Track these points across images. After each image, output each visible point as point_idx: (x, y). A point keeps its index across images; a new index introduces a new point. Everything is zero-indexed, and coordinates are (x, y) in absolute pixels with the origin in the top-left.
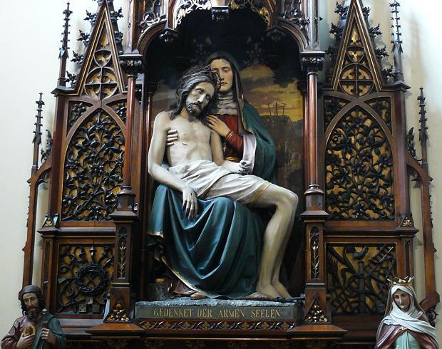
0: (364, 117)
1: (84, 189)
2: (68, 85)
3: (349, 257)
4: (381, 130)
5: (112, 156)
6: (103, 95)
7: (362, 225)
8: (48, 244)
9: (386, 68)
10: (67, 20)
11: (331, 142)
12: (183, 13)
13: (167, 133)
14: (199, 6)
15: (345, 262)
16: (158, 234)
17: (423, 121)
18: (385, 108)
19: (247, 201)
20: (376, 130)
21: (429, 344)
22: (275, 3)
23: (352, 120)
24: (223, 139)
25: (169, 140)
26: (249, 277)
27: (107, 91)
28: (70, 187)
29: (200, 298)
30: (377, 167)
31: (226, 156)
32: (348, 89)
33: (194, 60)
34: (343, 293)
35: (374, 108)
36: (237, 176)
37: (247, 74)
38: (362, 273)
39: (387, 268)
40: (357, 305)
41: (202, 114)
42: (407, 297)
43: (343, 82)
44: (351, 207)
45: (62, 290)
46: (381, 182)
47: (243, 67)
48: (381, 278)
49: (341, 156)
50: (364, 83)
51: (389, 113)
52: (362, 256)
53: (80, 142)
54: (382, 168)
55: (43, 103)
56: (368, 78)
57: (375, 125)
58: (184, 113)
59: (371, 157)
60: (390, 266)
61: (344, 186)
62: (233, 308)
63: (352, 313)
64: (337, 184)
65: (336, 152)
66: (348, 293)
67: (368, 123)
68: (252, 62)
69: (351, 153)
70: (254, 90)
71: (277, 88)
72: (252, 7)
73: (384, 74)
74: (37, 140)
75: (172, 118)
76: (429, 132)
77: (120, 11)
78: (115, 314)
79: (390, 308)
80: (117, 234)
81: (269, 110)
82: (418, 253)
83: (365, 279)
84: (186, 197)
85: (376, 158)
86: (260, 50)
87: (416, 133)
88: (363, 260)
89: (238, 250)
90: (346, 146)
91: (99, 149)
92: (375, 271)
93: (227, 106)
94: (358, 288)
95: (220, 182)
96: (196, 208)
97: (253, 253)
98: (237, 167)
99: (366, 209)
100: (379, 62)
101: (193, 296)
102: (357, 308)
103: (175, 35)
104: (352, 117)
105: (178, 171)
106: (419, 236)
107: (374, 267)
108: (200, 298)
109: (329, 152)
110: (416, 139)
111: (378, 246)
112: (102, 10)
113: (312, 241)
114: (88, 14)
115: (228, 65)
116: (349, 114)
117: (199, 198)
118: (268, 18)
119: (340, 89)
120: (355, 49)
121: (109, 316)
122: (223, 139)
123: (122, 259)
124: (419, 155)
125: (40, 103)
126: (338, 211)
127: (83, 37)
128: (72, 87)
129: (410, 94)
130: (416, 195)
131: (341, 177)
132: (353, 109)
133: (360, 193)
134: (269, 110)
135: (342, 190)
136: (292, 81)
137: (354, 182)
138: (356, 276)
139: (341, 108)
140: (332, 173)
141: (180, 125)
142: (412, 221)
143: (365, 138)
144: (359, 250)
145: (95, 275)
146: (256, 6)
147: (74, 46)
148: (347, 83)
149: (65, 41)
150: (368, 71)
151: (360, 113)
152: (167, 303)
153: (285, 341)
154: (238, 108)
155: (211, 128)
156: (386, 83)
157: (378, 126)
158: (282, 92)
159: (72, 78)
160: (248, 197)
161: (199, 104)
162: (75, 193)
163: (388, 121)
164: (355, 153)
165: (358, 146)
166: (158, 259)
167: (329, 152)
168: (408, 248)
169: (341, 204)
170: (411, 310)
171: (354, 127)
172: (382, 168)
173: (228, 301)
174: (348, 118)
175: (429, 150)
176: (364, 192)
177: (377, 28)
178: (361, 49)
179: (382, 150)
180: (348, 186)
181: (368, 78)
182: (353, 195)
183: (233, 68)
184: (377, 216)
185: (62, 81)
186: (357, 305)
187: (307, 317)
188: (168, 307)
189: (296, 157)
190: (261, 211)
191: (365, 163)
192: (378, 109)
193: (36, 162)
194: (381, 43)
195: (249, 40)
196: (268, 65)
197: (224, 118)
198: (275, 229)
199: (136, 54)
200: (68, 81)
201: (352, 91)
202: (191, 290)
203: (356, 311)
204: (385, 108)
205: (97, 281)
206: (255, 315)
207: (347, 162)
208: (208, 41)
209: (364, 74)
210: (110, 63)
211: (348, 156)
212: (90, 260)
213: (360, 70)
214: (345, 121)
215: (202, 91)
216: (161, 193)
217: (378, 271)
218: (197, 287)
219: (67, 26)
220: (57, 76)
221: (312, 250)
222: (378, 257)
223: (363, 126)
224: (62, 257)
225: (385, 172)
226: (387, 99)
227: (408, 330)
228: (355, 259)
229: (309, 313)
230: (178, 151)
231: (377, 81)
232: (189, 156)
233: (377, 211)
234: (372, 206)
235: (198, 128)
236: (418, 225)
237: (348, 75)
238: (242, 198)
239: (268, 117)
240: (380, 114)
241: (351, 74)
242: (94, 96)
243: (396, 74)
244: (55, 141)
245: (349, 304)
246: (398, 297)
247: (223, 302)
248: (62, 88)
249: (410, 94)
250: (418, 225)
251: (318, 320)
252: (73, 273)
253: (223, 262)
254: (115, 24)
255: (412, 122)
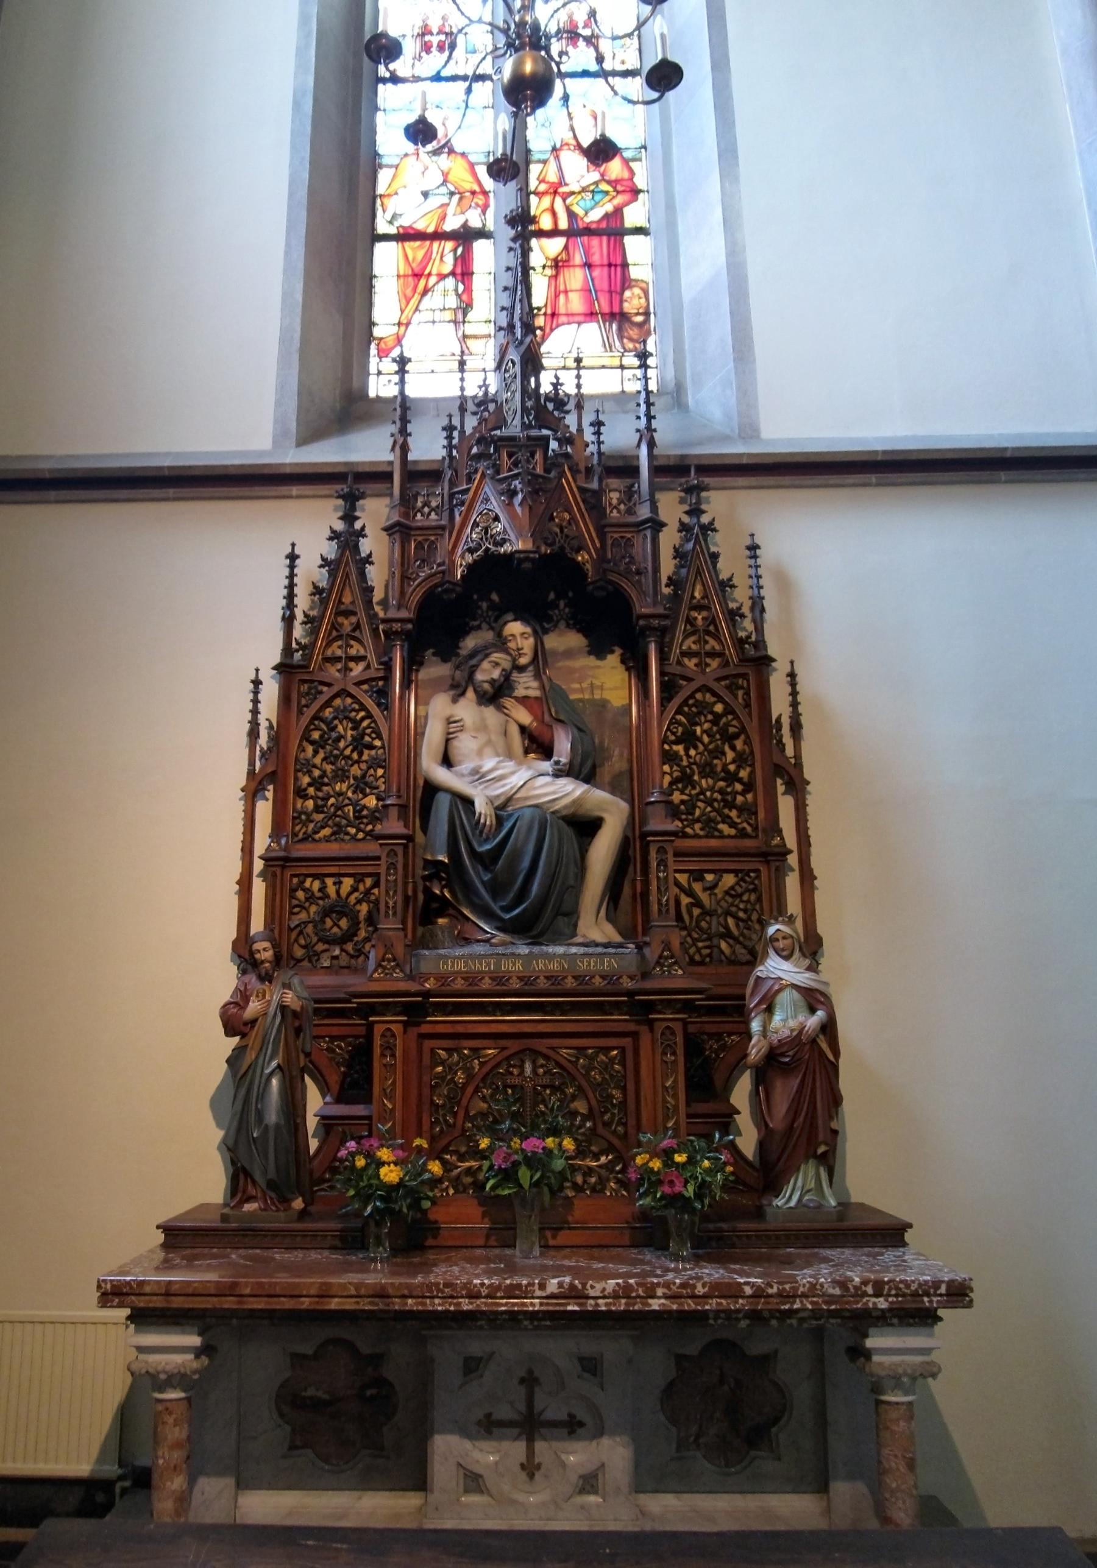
0: (713, 699)
1: (323, 799)
2: (298, 656)
3: (697, 887)
4: (737, 718)
5: (361, 754)
6: (347, 669)
7: (714, 843)
8: (274, 875)
9: (742, 634)
10: (292, 567)
11: (669, 733)
12: (469, 558)
13: (449, 721)
14: (493, 548)
15: (690, 893)
16: (441, 858)
17: (795, 704)
18: (742, 688)
19: (564, 813)
20: (730, 717)
21: (822, 1003)
22: (598, 545)
23: (697, 704)
24: (523, 729)
25: (451, 730)
26: (566, 915)
27: (352, 664)
28: (301, 797)
29: (503, 944)
30: (732, 767)
31: (527, 752)
32: (691, 663)
33: (476, 623)
34: (689, 935)
35: (727, 687)
36: (548, 779)
37: (552, 641)
38: (713, 907)
39: (748, 901)
40: (708, 951)
41: (495, 695)
42: (789, 941)
43: (684, 654)
44: (698, 821)
45: (294, 935)
46: (739, 787)
47: (546, 631)
48: (741, 914)
49: (682, 753)
50: (712, 654)
51: (747, 693)
52: (715, 886)
53: (316, 735)
54: (739, 767)
55: (261, 683)
56: (717, 647)
57: (729, 710)
58: (470, 694)
59: (724, 754)
60: (753, 897)
61: (687, 792)
62: (552, 957)
63: (701, 963)
64: (678, 789)
65: (675, 748)
66: (695, 936)
67: (719, 708)
68: (555, 626)
69: (696, 748)
70: (560, 664)
71: (592, 661)
72: (568, 550)
73: (741, 642)
74: (253, 734)
75: (455, 700)
76: (803, 720)
77: (370, 555)
78: (384, 968)
79: (766, 955)
80: (384, 858)
81: (582, 690)
82: (792, 882)
83: (719, 916)
84: (480, 806)
85: (730, 755)
86: (567, 610)
87: (786, 722)
88: (716, 891)
89: (552, 878)
90: (689, 739)
91: (342, 744)
92: (732, 905)
93: (526, 685)
94: (710, 928)
95: (527, 786)
96: (494, 822)
97: (572, 882)
98: (546, 766)
99: (718, 823)
100: (734, 626)
101: (493, 941)
102: (710, 955)
103: (458, 589)
104: (697, 701)
105: (465, 772)
106: (793, 860)
107: (730, 900)
108: (503, 944)
109: (666, 747)
110: (786, 730)
111: (735, 872)
112: (342, 555)
113: (658, 865)
114: (323, 559)
115: (528, 630)
116: (692, 696)
117: (497, 808)
118: (588, 566)
119: (679, 663)
120: (699, 608)
121: (376, 970)
122: (523, 729)
123: (391, 893)
124: (790, 751)
125: (257, 683)
126: (680, 825)
127: (317, 590)
128: (303, 659)
129: (775, 670)
130: (786, 805)
131: (685, 780)
132: (698, 690)
133: (709, 802)
134: (582, 690)
135: (685, 797)
136: (612, 652)
137: (701, 787)
138: (706, 913)
139: (681, 687)
140: (671, 774)
141: (467, 710)
142: (782, 839)
143: (715, 729)
144: (709, 877)
145: (341, 914)
146: (572, 549)
147: (303, 602)
148: (689, 654)
149: (290, 597)
150: (720, 641)
151: (708, 695)
152: (459, 952)
153: (623, 1002)
154: (542, 687)
155: (507, 715)
156: (743, 653)
157: (733, 712)
158: (599, 667)
159: (302, 647)
160: (566, 807)
161: (492, 682)
162: (310, 804)
163: (747, 705)
164: (701, 748)
165: (706, 739)
166: (438, 892)
167: (666, 747)
168: (781, 872)
169: (684, 817)
170: (794, 957)
171: (700, 713)
172: (739, 767)
173: (544, 948)
174: (691, 702)
175: (805, 746)
176: (716, 800)
177: (730, 579)
178: (707, 608)
179: (739, 744)
180: (694, 792)
181: (717, 647)
182: (700, 804)
183: (535, 633)
184: (733, 832)
185: (287, 651)
186: (708, 951)
187: (654, 968)
188: (460, 958)
189: (621, 755)
190: (585, 826)
191: (715, 761)
192: (732, 689)
193: (252, 763)
194: (734, 600)
195: (552, 596)
196: (579, 631)
197: (524, 701)
198: (603, 850)
199: (404, 614)
200: (297, 651)
201: (696, 665)
202: (488, 933)
203: (708, 959)
204: (742, 688)
205: (344, 923)
206: (583, 966)
207: (692, 760)
208: (495, 597)
209: (712, 642)
210: (357, 627)
211: (692, 752)
212: (333, 895)
213: (707, 638)
214: (688, 705)
215: (497, 664)
216: (443, 803)
217: (737, 906)
218: (498, 929)
219: (291, 576)
220: (279, 644)
221: (658, 877)
222: (737, 888)
223: (712, 713)
224: (293, 890)
225: (743, 774)
226: (744, 676)
227: (794, 986)
228: (705, 889)
229: (658, 963)
230: (465, 744)
231: (731, 651)
232: (480, 753)
233: (733, 825)
234: (726, 819)
235: (490, 714)
236: (791, 842)
237: (690, 644)
238: (557, 807)
239: (580, 700)
240: (736, 697)
241: (694, 643)
242: (333, 671)
243: (757, 641)
244: (278, 737)
245: (699, 950)
246: (778, 940)
247: (536, 949)
248: (288, 661)
249: (775, 670)
250: (791, 842)
251: (669, 972)
252: (308, 913)
253: (536, 896)
254: (362, 575)
255: (779, 706)
